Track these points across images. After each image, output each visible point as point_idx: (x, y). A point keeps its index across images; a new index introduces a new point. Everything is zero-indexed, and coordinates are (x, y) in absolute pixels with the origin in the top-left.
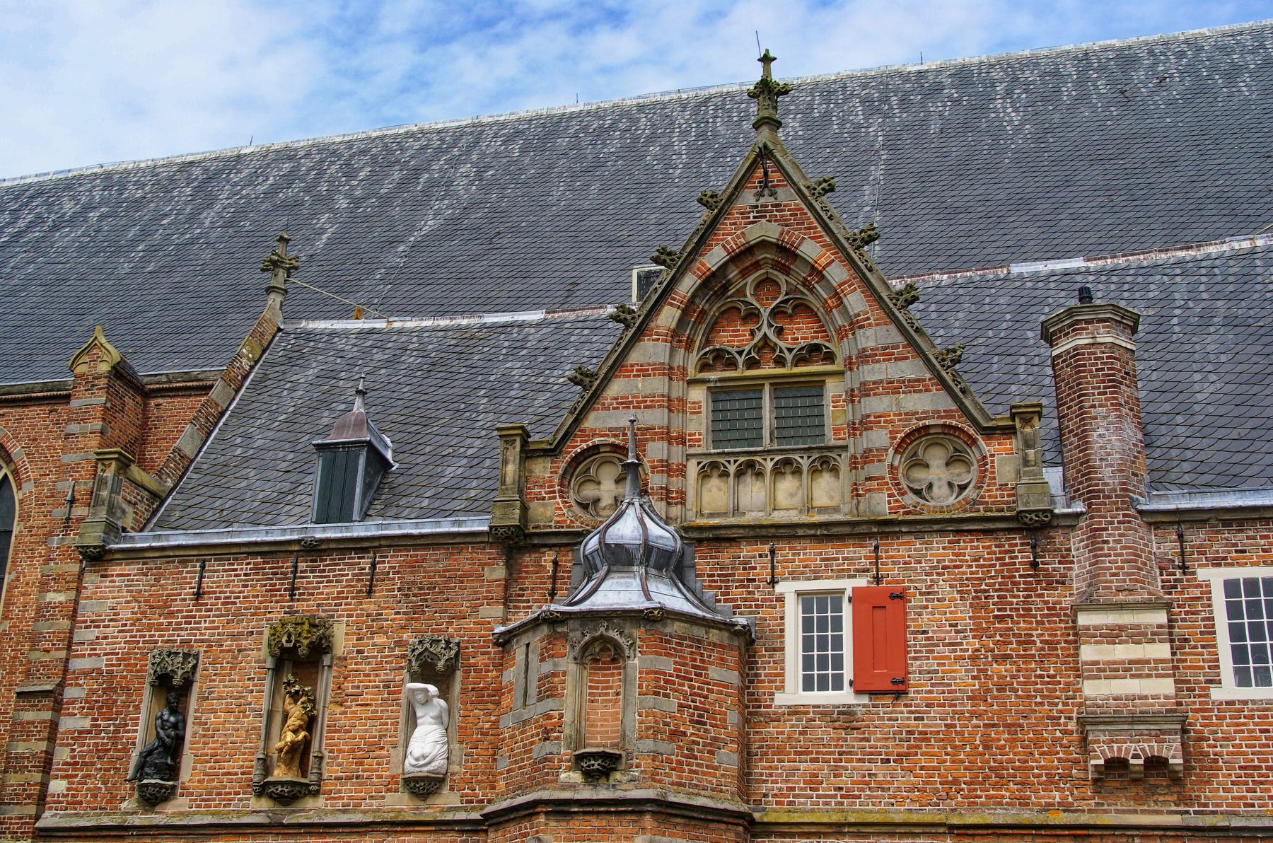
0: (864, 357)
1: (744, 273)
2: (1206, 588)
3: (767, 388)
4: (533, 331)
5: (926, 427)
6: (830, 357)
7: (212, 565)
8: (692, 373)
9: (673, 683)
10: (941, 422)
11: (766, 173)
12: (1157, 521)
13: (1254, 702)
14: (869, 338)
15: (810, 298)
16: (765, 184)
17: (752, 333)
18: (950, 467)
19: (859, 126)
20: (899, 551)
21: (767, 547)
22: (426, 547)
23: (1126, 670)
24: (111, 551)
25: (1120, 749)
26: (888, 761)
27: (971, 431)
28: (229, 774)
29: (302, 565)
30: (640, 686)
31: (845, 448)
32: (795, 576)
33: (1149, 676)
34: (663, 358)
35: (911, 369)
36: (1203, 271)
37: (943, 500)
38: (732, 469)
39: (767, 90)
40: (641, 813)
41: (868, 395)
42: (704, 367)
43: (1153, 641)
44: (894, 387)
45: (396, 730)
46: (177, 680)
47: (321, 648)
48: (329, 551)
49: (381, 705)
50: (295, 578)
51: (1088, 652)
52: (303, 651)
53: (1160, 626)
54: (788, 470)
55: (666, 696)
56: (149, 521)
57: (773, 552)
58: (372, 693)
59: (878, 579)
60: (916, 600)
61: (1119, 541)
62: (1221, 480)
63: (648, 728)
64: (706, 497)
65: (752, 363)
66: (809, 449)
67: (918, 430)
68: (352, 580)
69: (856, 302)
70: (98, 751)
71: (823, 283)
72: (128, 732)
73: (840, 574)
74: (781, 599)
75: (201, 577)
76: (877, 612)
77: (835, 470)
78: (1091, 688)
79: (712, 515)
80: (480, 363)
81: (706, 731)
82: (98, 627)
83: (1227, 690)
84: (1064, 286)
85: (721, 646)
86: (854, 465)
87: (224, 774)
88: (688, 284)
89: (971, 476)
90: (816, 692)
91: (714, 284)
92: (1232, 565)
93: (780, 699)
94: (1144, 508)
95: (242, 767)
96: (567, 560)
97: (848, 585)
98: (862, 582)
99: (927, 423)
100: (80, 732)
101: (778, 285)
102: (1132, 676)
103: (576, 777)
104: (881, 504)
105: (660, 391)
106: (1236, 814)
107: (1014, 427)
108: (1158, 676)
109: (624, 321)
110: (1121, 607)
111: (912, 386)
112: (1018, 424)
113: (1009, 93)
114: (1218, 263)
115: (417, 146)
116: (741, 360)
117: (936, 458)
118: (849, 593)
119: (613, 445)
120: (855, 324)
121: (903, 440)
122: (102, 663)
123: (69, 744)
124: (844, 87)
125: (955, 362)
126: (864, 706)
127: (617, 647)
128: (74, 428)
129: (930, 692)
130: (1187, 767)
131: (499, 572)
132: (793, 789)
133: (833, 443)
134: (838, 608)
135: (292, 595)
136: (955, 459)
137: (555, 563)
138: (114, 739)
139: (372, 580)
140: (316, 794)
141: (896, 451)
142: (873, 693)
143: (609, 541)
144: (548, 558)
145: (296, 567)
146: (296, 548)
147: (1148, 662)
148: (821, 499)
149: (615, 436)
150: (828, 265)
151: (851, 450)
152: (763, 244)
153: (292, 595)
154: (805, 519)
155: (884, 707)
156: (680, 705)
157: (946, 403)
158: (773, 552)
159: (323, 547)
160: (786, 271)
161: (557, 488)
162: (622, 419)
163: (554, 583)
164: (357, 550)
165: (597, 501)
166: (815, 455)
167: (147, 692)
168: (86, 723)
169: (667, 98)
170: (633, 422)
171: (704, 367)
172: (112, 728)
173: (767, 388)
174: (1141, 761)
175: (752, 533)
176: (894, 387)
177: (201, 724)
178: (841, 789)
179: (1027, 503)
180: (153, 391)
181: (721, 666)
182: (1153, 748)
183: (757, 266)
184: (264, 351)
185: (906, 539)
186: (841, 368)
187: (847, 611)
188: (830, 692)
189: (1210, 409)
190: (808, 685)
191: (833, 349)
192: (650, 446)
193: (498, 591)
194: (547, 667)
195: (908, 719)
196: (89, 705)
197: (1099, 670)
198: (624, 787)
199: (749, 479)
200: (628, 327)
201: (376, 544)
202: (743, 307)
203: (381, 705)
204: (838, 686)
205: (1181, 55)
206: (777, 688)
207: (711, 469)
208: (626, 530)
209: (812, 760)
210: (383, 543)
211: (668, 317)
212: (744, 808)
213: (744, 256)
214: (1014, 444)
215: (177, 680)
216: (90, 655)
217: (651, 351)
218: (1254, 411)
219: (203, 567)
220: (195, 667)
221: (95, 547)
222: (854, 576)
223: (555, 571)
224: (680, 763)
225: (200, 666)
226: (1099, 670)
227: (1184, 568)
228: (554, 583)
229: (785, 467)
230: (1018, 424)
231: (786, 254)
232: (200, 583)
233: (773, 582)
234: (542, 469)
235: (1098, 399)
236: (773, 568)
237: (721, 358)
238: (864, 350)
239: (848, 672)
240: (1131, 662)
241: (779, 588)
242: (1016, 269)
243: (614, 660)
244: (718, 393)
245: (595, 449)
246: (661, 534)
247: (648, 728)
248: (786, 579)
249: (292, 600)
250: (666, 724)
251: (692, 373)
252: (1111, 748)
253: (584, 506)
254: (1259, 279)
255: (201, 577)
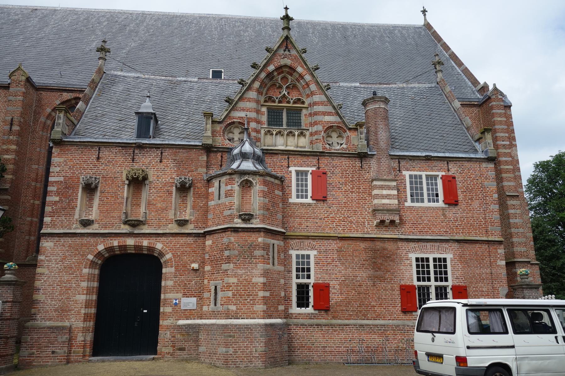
0: (315, 104)
1: (279, 74)
2: (405, 176)
3: (285, 111)
4: (195, 84)
5: (332, 126)
6: (303, 103)
7: (103, 149)
8: (262, 103)
9: (267, 194)
10: (337, 125)
11: (287, 44)
12: (393, 157)
13: (415, 207)
14: (317, 98)
15: (298, 84)
16: (287, 47)
17: (280, 93)
18: (338, 138)
19: (270, 35)
20: (324, 161)
21: (287, 157)
22: (180, 148)
23: (386, 197)
24: (65, 141)
25: (384, 218)
26: (321, 219)
27: (345, 128)
28: (113, 217)
29: (136, 151)
30: (259, 195)
31: (308, 130)
32: (295, 165)
33: (392, 199)
34: (255, 97)
35: (329, 109)
36: (392, 91)
37: (336, 148)
38: (274, 133)
39: (287, 18)
40: (260, 231)
41: (316, 115)
42: (265, 101)
43: (393, 190)
44: (324, 114)
45: (171, 205)
46: (93, 186)
47: (145, 178)
48: (146, 148)
49: (166, 197)
50: (134, 155)
51: (375, 192)
52: (140, 178)
53: (395, 186)
54: (291, 134)
55: (266, 198)
56: (72, 132)
57: (288, 158)
58: (163, 193)
59: (319, 168)
60: (329, 174)
61: (385, 163)
62: (406, 148)
63: (261, 207)
64: (266, 140)
65: (280, 102)
66: (298, 129)
67: (330, 126)
68: (154, 157)
69: (313, 87)
70: (62, 208)
71: (303, 80)
72: (74, 202)
73: (308, 166)
74: (291, 172)
75: (99, 153)
76: (319, 177)
77: (305, 136)
78: (376, 201)
79: (268, 146)
80: (179, 92)
81: (275, 209)
82: (60, 167)
83: (409, 203)
84: (355, 90)
85: (278, 184)
86: (311, 134)
87: (111, 217)
88: (263, 75)
89: (344, 141)
90: (300, 199)
91: (270, 76)
92: (411, 171)
93: (291, 201)
94: (392, 154)
95: (117, 215)
96: (226, 156)
97: (310, 169)
98: (314, 169)
99: (333, 125)
100: (55, 202)
101: (287, 78)
102: (387, 199)
103: (240, 221)
104: (319, 147)
105: (254, 107)
106: (410, 235)
107: (357, 128)
108: (394, 199)
109: (242, 84)
110: (385, 180)
111: (329, 114)
112: (359, 128)
113: (313, 33)
114: (395, 89)
115: (123, 17)
116: (277, 101)
117: (334, 135)
118: (310, 171)
119: (239, 122)
120: (312, 94)
121: (326, 129)
122: (62, 179)
123: (51, 206)
124: (264, 23)
125: (340, 108)
126: (315, 204)
127: (251, 182)
128: (11, 98)
129: (333, 201)
130: (400, 224)
131: (205, 158)
132: (294, 226)
133: (304, 128)
134: (306, 175)
135: (133, 161)
136: (340, 136)
137: (222, 157)
138: (69, 204)
139: (161, 158)
140: (144, 224)
141: (324, 132)
142: (316, 200)
143: (243, 151)
144: (219, 155)
145: (134, 152)
146: (134, 145)
147: (391, 195)
148: (301, 144)
149: (240, 119)
150: (305, 75)
151: (310, 130)
152: (286, 66)
153: (133, 161)
154: (295, 149)
155: (320, 204)
156: (269, 201)
157: (339, 120)
158: (288, 158)
159: (145, 146)
160: (291, 75)
161: (222, 134)
162: (242, 114)
163: (221, 163)
164: (156, 148)
165: (233, 139)
166: (299, 131)
167: (80, 190)
168: (57, 199)
169: (208, 16)
170: (246, 115)
171: (265, 101)
172: (67, 201)
173: (285, 110)
174: (389, 221)
175: (282, 152)
176: (324, 114)
177: (102, 201)
178: (308, 226)
179: (361, 150)
180: (39, 88)
181: (278, 190)
182: (392, 218)
183: (282, 72)
184: (101, 79)
185: (327, 157)
186: (307, 106)
187: (310, 177)
188: (304, 199)
189: (400, 129)
190: (298, 197)
191: (305, 100)
192: (251, 123)
193: (204, 164)
194: (229, 187)
195: (327, 208)
196: (58, 193)
197: (379, 197)
198: (256, 224)
199: (278, 136)
200: (243, 86)
201: (163, 146)
202: (278, 85)
203: (166, 197)
204: (306, 197)
205: (359, 29)
206: (290, 198)
207: (269, 133)
208: (247, 148)
209: (300, 218)
210: (165, 146)
211: (257, 85)
212: (283, 230)
213: (279, 69)
214: (356, 133)
215: (93, 186)
216: (57, 176)
217: (252, 94)
218: (411, 131)
219: (99, 149)
220: (99, 182)
221: (58, 140)
222: (312, 167)
223: (222, 159)
224: (269, 217)
225: (100, 182)
226: (379, 197)
227: (399, 171)
228: (221, 163)
229: (291, 134)
230: (359, 128)
231: (292, 70)
232: (99, 155)
233: (288, 167)
234: (218, 127)
235: (380, 123)
236: (288, 163)
237: (270, 99)
238: (316, 102)
239: (310, 194)
240: (387, 195)
241: (290, 169)
242: (341, 84)
243: (249, 187)
244: (270, 110)
245: (234, 123)
246: (258, 152)
247: (261, 207)
248: (292, 166)
249: (133, 162)
250: (266, 206)
251: (262, 103)
252: (381, 217)
253: (230, 140)
254: (407, 95)
255: (99, 153)
